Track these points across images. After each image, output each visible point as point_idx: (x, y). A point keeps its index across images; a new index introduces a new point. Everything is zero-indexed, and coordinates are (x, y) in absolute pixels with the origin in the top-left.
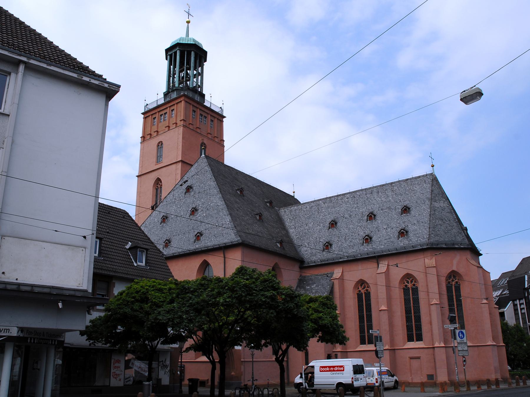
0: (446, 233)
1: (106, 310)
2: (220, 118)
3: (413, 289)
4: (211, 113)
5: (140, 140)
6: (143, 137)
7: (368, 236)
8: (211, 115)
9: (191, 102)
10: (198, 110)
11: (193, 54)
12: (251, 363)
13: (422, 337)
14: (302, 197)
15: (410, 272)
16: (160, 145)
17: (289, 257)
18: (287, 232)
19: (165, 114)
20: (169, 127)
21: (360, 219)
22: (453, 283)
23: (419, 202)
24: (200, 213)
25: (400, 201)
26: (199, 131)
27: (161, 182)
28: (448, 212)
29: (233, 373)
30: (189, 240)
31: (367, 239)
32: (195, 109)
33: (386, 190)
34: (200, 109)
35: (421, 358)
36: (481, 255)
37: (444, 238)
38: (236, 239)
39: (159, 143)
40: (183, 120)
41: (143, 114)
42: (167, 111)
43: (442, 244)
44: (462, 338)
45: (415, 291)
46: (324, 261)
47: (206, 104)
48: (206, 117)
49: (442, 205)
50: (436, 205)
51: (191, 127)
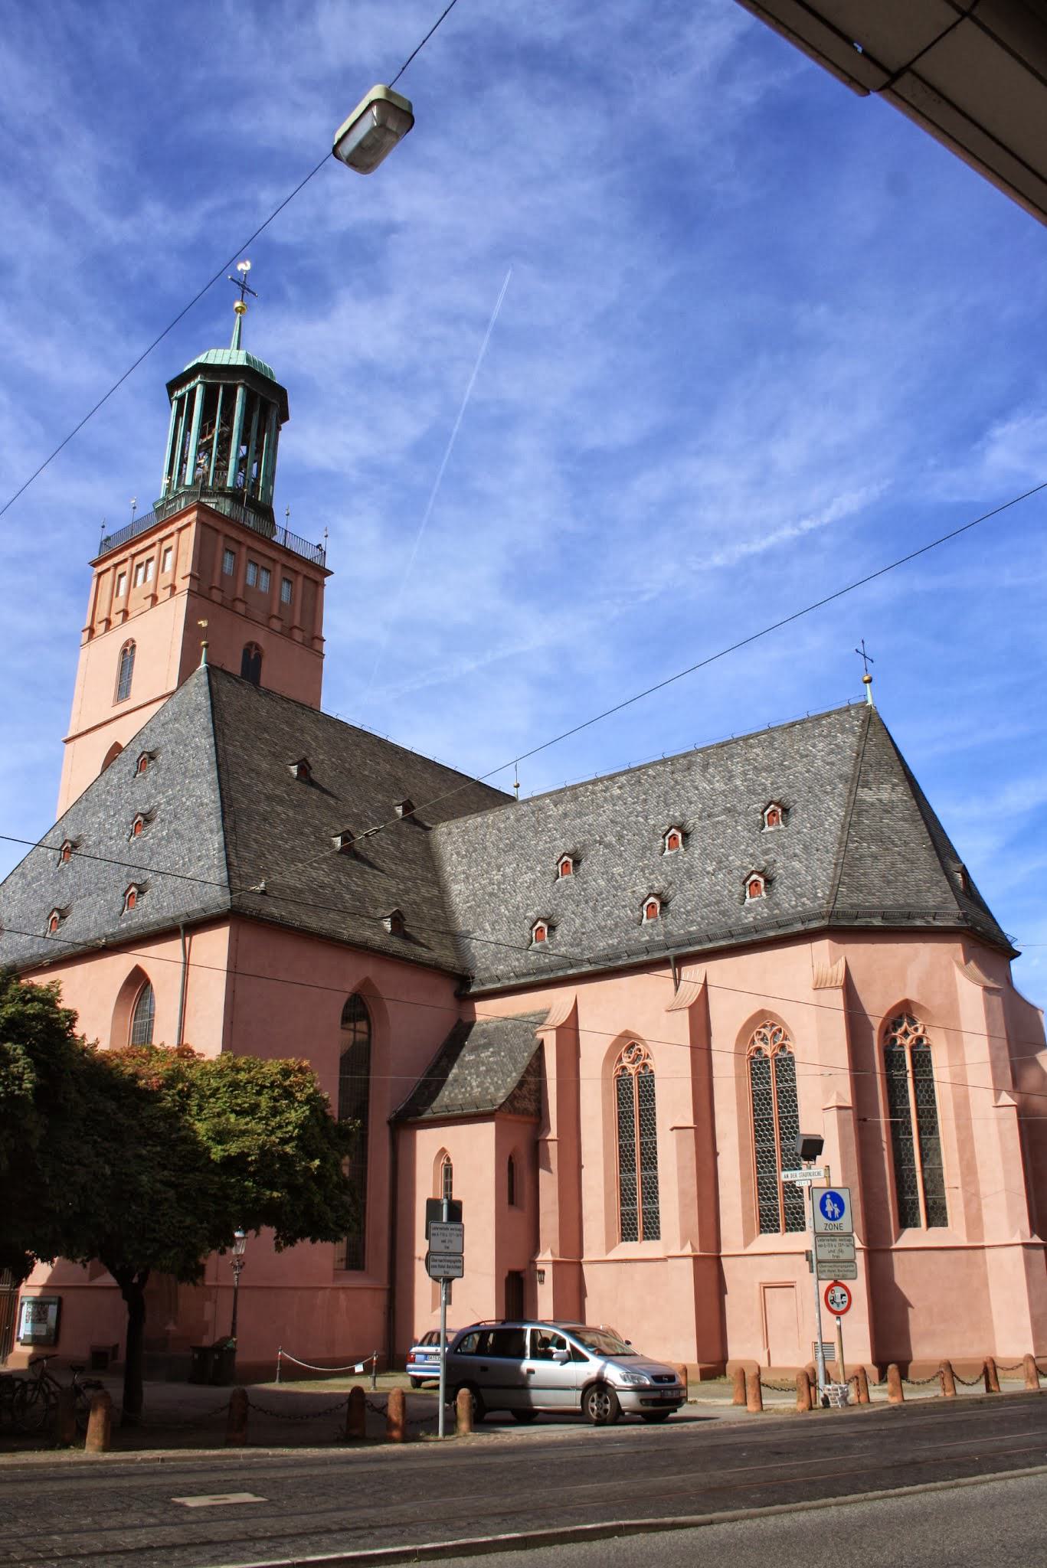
0: (889, 882)
2: (312, 574)
3: (779, 1061)
4: (283, 559)
8: (284, 566)
10: (244, 550)
13: (945, 1219)
14: (522, 795)
15: (771, 1006)
16: (128, 651)
17: (393, 956)
18: (443, 891)
19: (149, 561)
21: (644, 847)
24: (154, 827)
25: (764, 790)
29: (171, 1327)
30: (111, 909)
33: (731, 756)
34: (249, 548)
35: (798, 1286)
36: (329, 573)
37: (878, 895)
38: (220, 900)
39: (126, 644)
42: (153, 552)
43: (871, 916)
44: (833, 1219)
45: (786, 1065)
46: (524, 975)
47: (278, 538)
49: (885, 796)
50: (867, 795)
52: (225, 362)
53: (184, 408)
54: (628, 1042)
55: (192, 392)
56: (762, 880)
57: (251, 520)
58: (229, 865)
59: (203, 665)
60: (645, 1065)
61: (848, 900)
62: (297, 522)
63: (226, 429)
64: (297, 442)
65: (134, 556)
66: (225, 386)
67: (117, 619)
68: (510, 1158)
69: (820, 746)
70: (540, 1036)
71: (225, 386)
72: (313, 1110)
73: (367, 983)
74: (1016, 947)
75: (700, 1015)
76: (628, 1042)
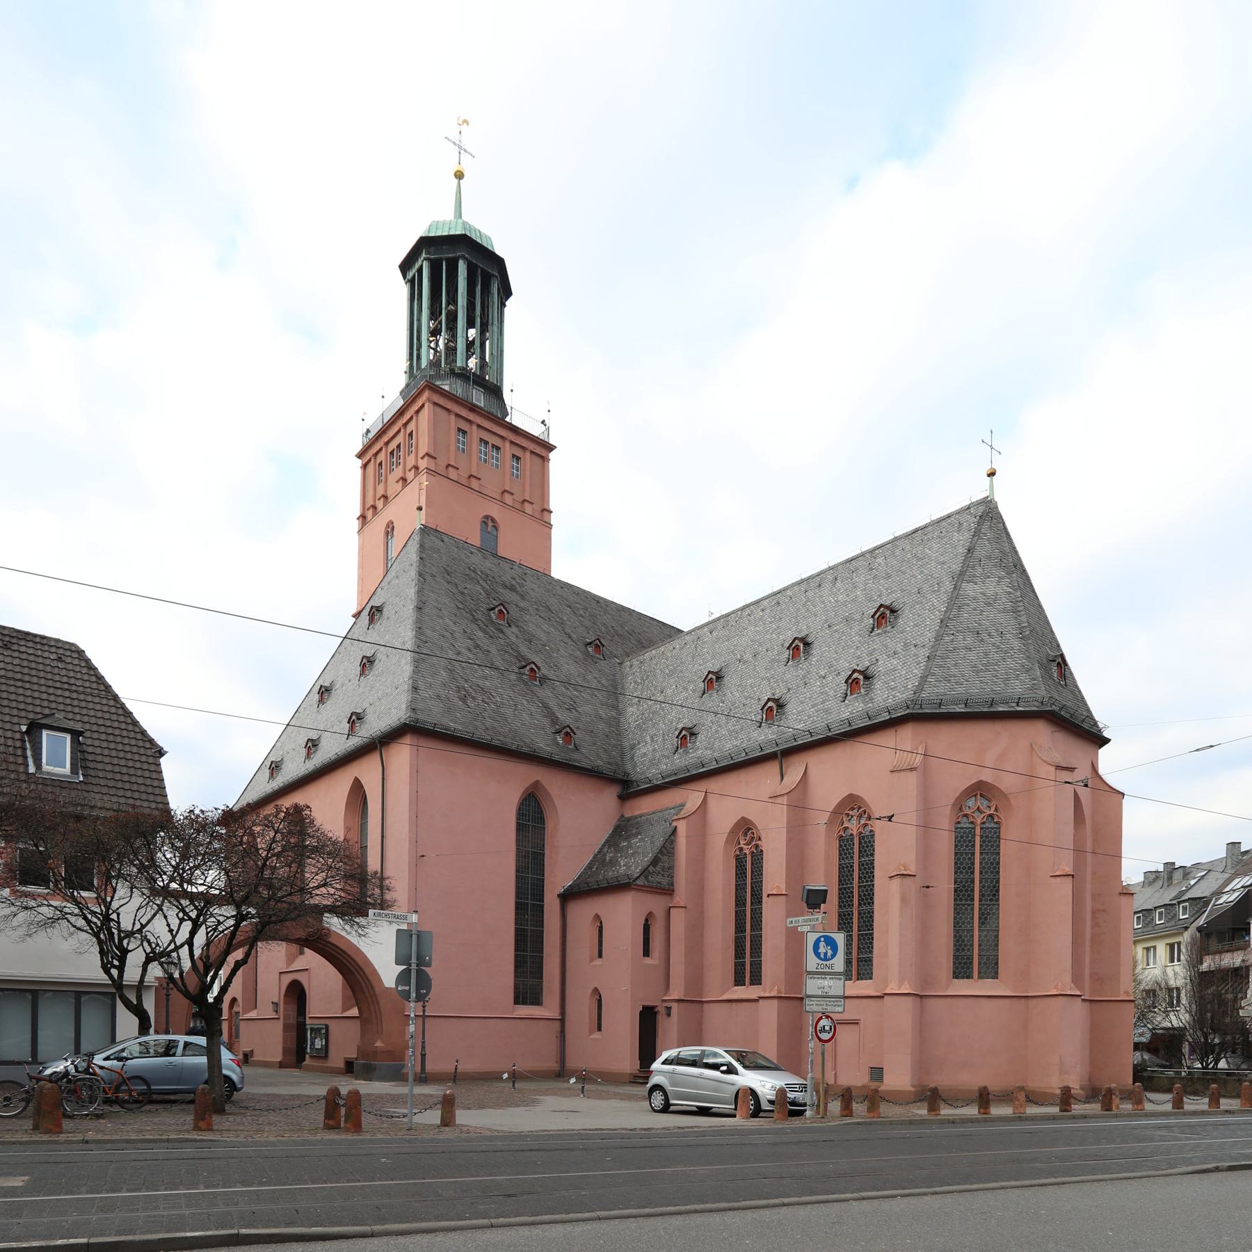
2: (539, 450)
4: (512, 437)
5: (356, 525)
6: (363, 517)
7: (776, 701)
9: (449, 405)
11: (462, 268)
12: (427, 1020)
22: (979, 819)
23: (926, 587)
26: (475, 484)
28: (1005, 611)
29: (379, 1044)
31: (771, 709)
32: (519, 453)
34: (479, 426)
36: (1106, 741)
37: (966, 684)
39: (388, 526)
40: (427, 454)
42: (399, 439)
44: (826, 959)
46: (669, 776)
48: (498, 449)
51: (453, 474)
52: (445, 233)
54: (745, 827)
55: (420, 271)
56: (861, 677)
57: (479, 398)
58: (415, 689)
60: (757, 846)
61: (935, 690)
63: (451, 307)
65: (387, 443)
66: (448, 260)
67: (380, 504)
68: (647, 920)
69: (936, 547)
70: (674, 824)
71: (448, 260)
73: (537, 784)
74: (1106, 734)
75: (798, 801)
76: (745, 827)
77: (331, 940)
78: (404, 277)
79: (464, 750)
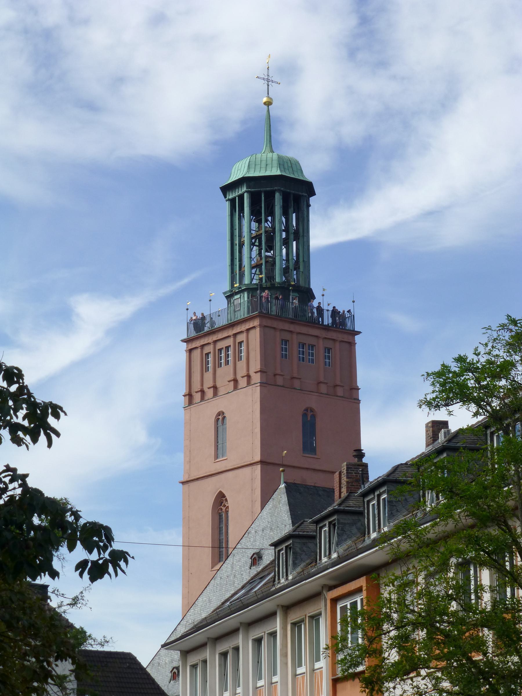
1: (460, 368)
5: (182, 400)
6: (190, 396)
11: (278, 197)
16: (220, 418)
20: (235, 381)
26: (297, 384)
27: (226, 500)
41: (184, 341)
42: (229, 342)
48: (313, 346)
53: (236, 206)
55: (241, 197)
59: (283, 486)
62: (328, 291)
64: (326, 229)
72: (273, 261)
77: (92, 646)
78: (225, 197)
79: (192, 378)
